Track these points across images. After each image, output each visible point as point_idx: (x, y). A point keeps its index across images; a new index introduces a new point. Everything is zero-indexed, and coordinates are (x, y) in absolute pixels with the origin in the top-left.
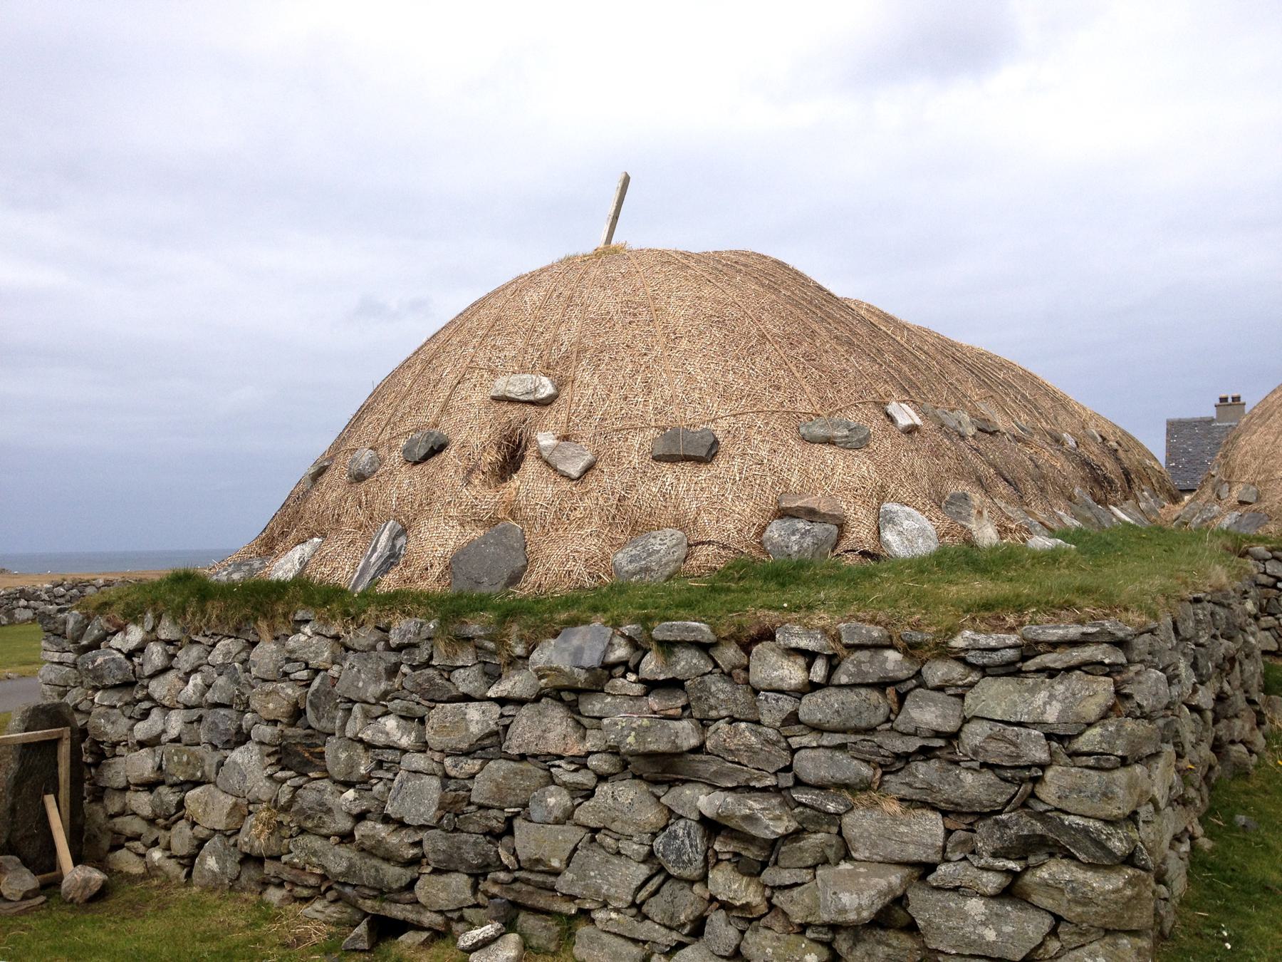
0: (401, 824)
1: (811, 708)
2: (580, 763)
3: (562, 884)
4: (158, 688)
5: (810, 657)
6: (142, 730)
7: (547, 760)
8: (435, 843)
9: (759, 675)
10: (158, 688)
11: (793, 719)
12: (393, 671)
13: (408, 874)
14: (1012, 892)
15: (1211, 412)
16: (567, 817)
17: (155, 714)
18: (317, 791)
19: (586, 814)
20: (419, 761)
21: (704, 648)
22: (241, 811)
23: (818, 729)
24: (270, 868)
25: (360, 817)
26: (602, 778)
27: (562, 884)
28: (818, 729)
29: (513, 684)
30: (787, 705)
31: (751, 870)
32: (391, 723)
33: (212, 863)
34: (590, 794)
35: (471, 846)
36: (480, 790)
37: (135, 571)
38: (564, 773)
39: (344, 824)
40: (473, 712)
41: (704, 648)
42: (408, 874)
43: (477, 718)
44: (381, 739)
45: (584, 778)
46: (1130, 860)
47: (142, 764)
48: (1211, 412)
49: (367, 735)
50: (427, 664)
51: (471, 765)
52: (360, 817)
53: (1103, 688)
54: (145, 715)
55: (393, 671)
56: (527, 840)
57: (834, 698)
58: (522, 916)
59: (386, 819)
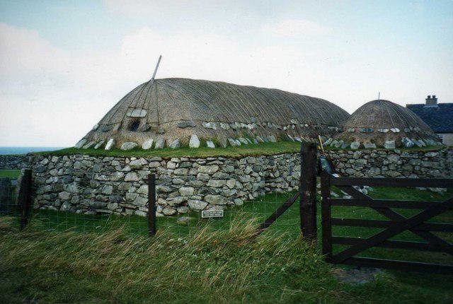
0: (105, 195)
1: (176, 172)
2: (138, 182)
3: (134, 203)
4: (52, 172)
5: (176, 163)
6: (48, 181)
7: (132, 182)
8: (112, 198)
9: (168, 166)
10: (52, 172)
11: (172, 173)
12: (104, 166)
13: (106, 204)
14: (203, 200)
15: (424, 102)
16: (135, 192)
17: (51, 178)
18: (88, 190)
19: (139, 191)
20: (109, 183)
21: (160, 162)
22: (72, 195)
23: (177, 175)
24: (78, 206)
25: (96, 194)
26: (141, 185)
27: (134, 203)
28: (177, 175)
29: (127, 169)
30: (172, 171)
31: (165, 198)
32: (103, 176)
33: (65, 206)
34: (139, 188)
35: (118, 197)
36: (120, 187)
37: (50, 150)
38: (135, 184)
39: (94, 196)
40: (119, 173)
41: (160, 162)
42: (106, 204)
43: (120, 175)
44: (101, 179)
45: (139, 185)
46: (219, 194)
47: (48, 188)
48: (424, 102)
49: (99, 178)
50: (110, 165)
51: (118, 183)
52: (96, 194)
53: (217, 168)
54: (49, 178)
55: (104, 166)
56: (128, 195)
57: (179, 170)
58: (127, 210)
59: (102, 194)
